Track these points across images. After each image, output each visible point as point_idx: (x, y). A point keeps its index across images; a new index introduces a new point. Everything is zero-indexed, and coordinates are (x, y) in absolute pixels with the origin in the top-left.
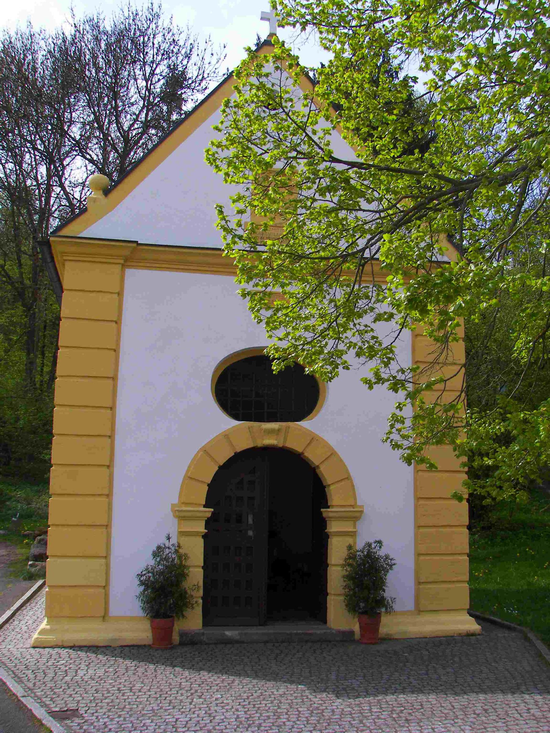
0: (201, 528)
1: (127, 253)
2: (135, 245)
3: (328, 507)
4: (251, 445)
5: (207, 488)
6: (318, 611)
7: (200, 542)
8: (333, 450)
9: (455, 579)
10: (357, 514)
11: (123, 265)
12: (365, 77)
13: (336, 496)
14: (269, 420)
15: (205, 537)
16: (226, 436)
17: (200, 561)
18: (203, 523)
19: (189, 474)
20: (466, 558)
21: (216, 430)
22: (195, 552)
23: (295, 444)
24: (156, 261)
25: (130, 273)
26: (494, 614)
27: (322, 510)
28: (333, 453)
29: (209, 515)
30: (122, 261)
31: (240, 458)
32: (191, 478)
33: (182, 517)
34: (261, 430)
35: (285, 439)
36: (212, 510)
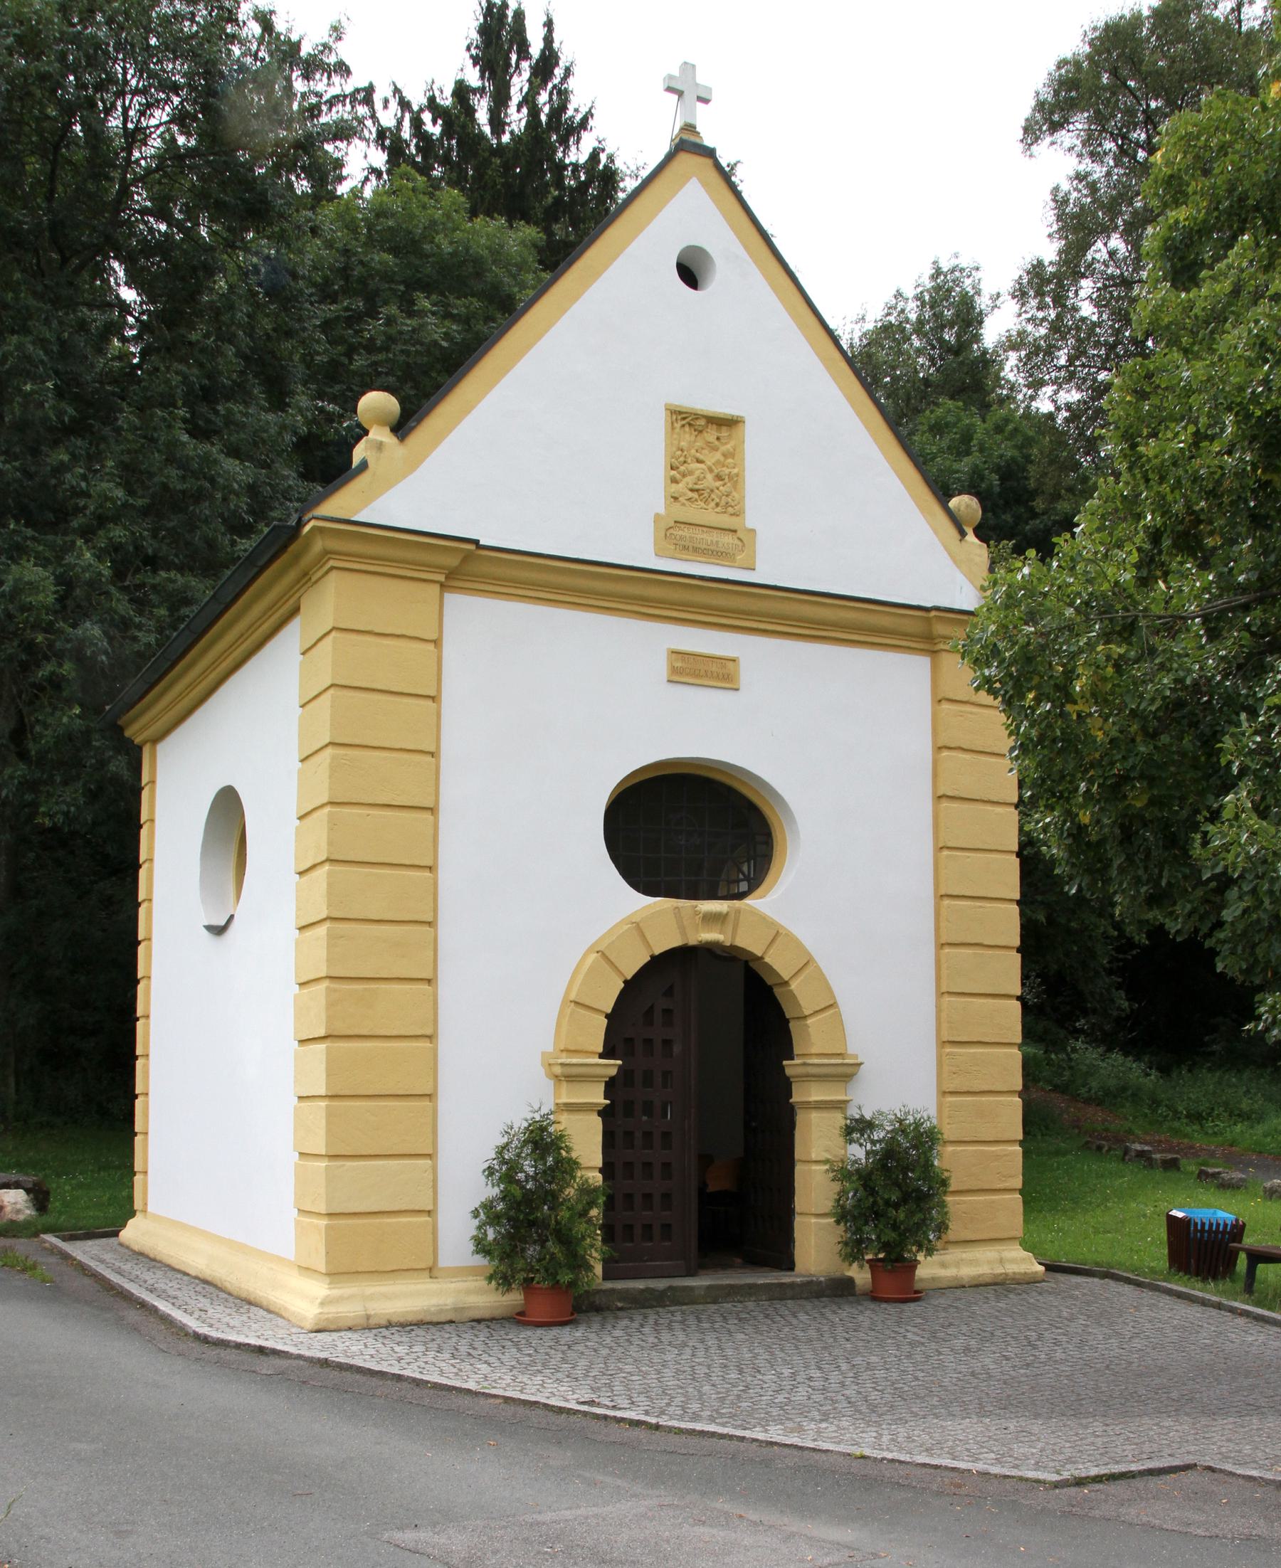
0: (597, 1096)
1: (453, 561)
2: (472, 547)
3: (792, 1059)
4: (676, 942)
5: (604, 1022)
6: (778, 1251)
7: (596, 1123)
8: (809, 954)
9: (1001, 1186)
10: (849, 1070)
11: (442, 585)
12: (1241, 460)
13: (812, 1041)
14: (713, 895)
15: (605, 1113)
16: (638, 927)
17: (598, 1161)
18: (602, 1087)
19: (573, 996)
20: (1018, 1149)
21: (613, 917)
22: (586, 1144)
23: (750, 942)
24: (497, 580)
25: (454, 601)
26: (696, 1417)
27: (785, 1063)
28: (809, 962)
29: (613, 1072)
30: (442, 578)
31: (660, 965)
32: (576, 1003)
33: (569, 1077)
34: (697, 913)
35: (734, 937)
36: (619, 1062)
